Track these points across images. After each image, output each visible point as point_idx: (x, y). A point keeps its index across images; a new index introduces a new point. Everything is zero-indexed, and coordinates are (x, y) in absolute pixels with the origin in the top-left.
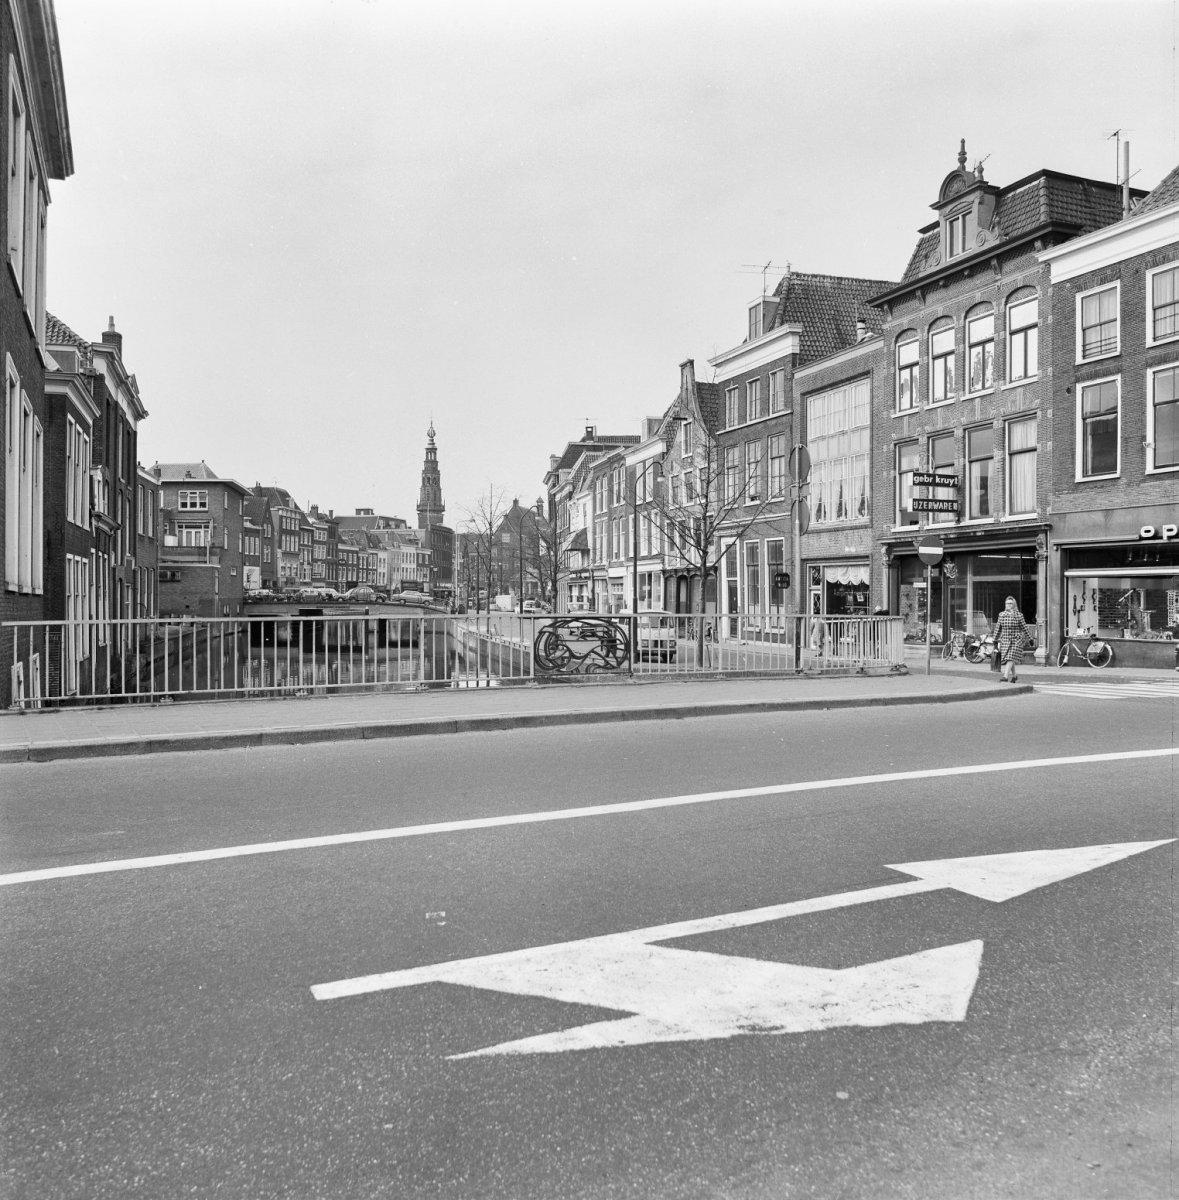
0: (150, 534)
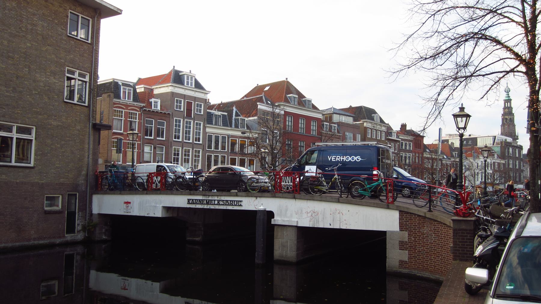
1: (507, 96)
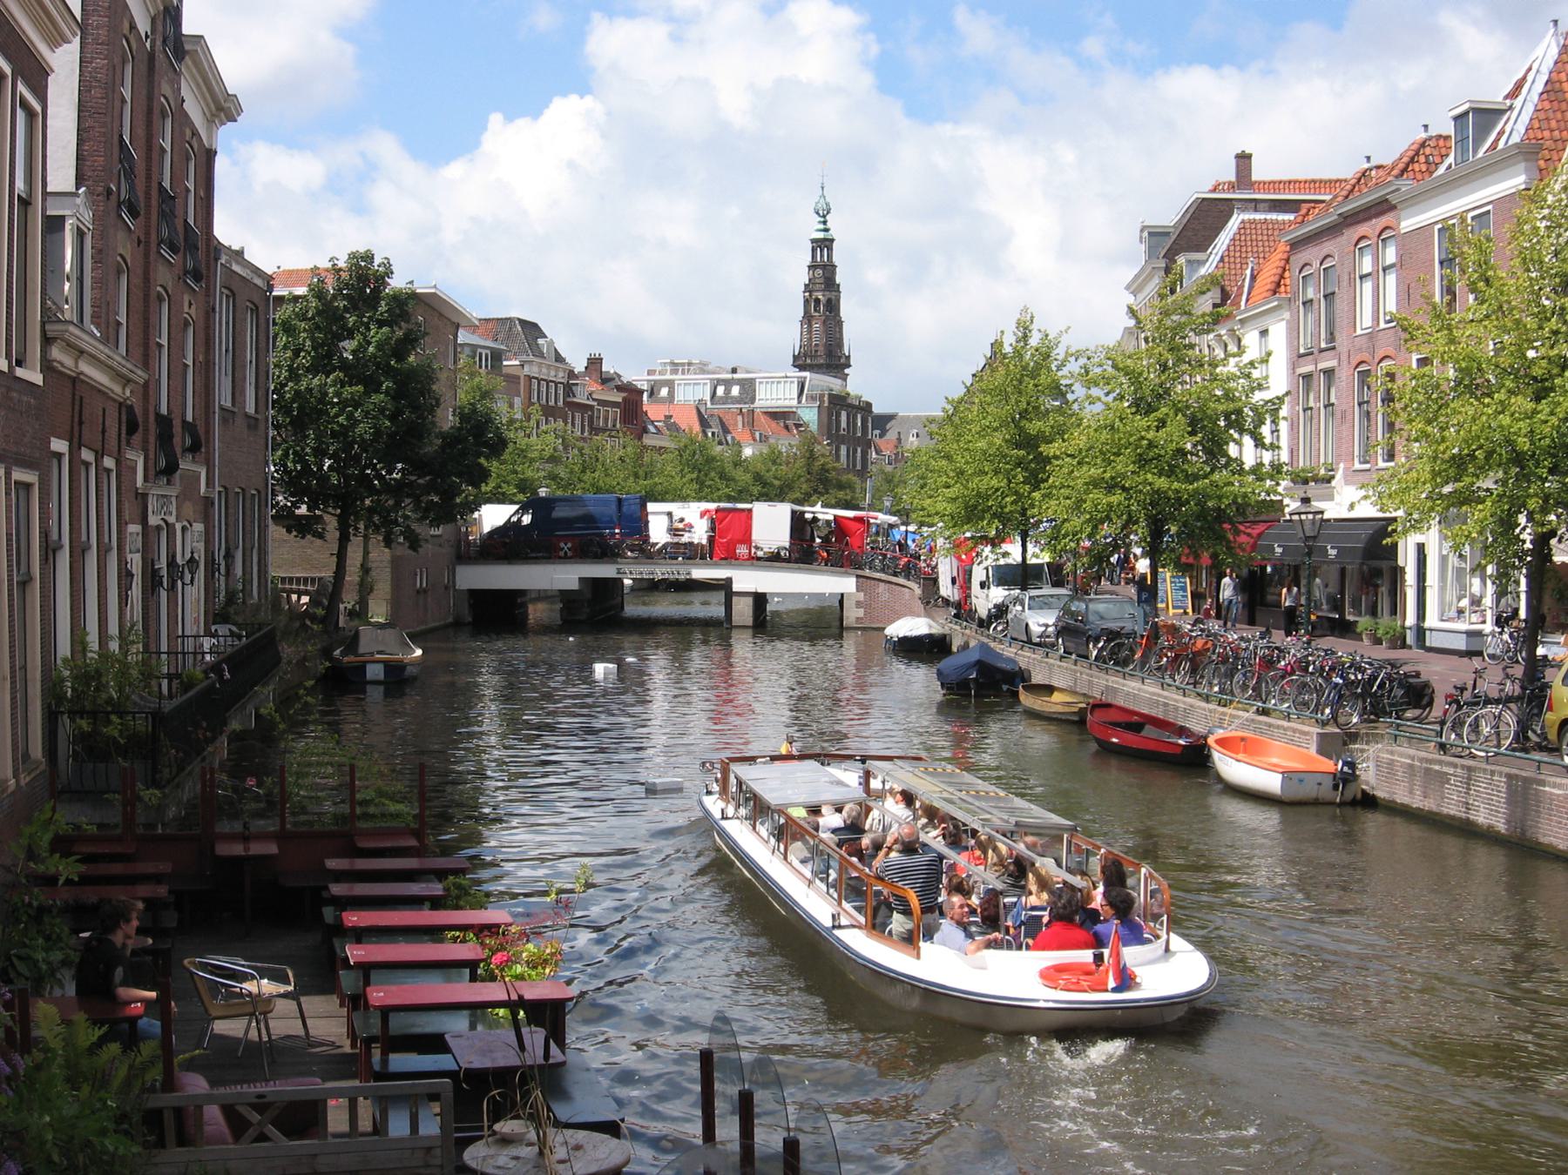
0: (250, 408)
1: (822, 226)
